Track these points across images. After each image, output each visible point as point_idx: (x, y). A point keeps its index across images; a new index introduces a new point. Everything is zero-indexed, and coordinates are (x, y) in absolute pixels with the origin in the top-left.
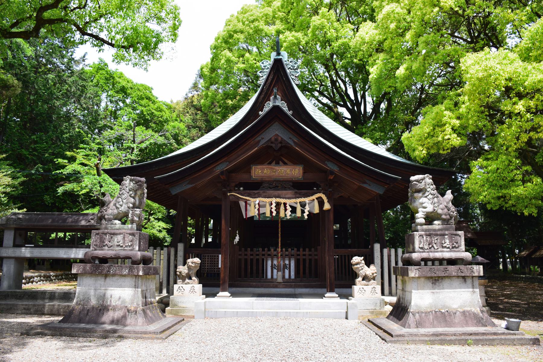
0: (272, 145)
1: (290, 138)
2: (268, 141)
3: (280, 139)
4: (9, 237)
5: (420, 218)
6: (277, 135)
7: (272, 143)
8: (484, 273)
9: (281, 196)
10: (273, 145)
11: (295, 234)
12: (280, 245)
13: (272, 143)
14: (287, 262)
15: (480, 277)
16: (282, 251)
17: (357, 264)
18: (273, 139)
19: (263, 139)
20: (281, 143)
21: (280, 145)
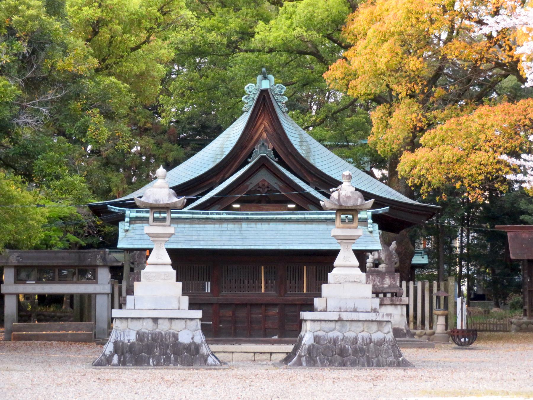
0: (259, 189)
1: (276, 183)
2: (256, 186)
3: (266, 184)
4: (8, 275)
6: (264, 180)
7: (259, 187)
8: (276, 335)
13: (259, 187)
15: (104, 355)
18: (261, 185)
19: (251, 184)
20: (268, 187)
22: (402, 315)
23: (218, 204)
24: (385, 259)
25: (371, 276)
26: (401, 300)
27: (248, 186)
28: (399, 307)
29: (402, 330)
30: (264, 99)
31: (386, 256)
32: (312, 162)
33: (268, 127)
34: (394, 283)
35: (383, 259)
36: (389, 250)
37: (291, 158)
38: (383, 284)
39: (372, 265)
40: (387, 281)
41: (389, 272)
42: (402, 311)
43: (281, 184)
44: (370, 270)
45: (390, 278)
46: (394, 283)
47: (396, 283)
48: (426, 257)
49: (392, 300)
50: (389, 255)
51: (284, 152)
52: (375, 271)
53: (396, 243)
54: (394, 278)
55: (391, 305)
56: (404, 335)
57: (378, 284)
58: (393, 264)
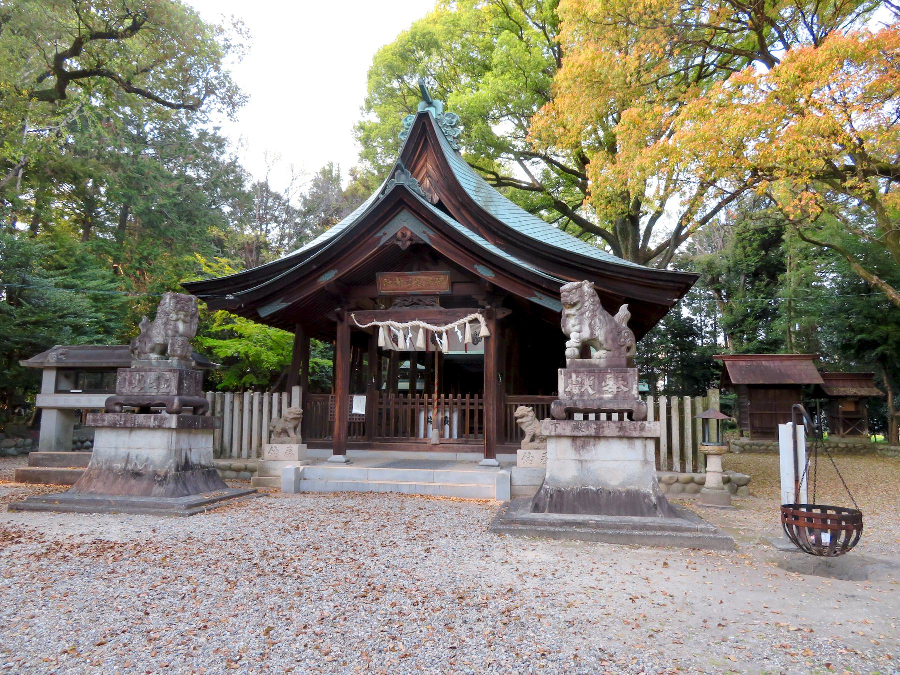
1: (424, 232)
3: (409, 234)
5: (572, 348)
6: (406, 228)
7: (399, 240)
9: (414, 322)
10: (400, 244)
11: (456, 377)
12: (436, 389)
13: (399, 240)
14: (448, 415)
16: (439, 397)
17: (523, 417)
19: (385, 234)
20: (411, 240)
21: (409, 243)
22: (646, 462)
23: (332, 269)
24: (606, 340)
25: (574, 376)
26: (642, 429)
27: (380, 238)
28: (639, 444)
29: (647, 496)
30: (424, 130)
31: (608, 333)
32: (493, 213)
33: (432, 171)
34: (626, 390)
35: (601, 339)
36: (612, 321)
37: (464, 212)
38: (600, 392)
39: (577, 352)
40: (611, 386)
41: (618, 368)
42: (645, 452)
43: (431, 234)
44: (572, 364)
45: (616, 378)
46: (626, 390)
47: (631, 390)
48: (647, 385)
49: (621, 429)
50: (615, 332)
51: (454, 205)
52: (583, 365)
53: (629, 309)
54: (624, 379)
55: (621, 438)
56: (652, 510)
57: (591, 392)
58: (624, 349)
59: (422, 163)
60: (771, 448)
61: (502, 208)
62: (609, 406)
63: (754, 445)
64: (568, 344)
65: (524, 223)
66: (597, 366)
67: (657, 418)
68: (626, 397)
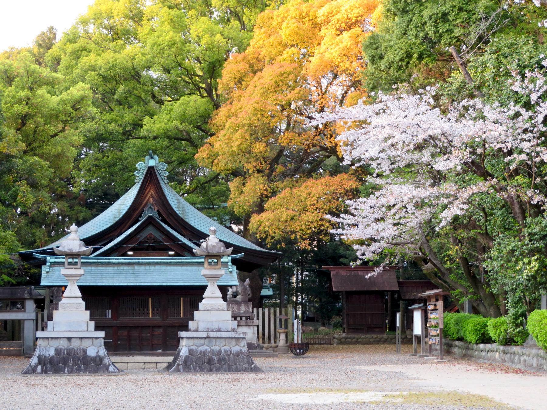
6: (151, 234)
20: (154, 239)
22: (254, 333)
26: (253, 322)
27: (139, 238)
28: (252, 327)
29: (254, 344)
32: (187, 220)
35: (240, 291)
36: (243, 285)
37: (171, 217)
38: (239, 310)
41: (244, 302)
49: (246, 322)
50: (245, 289)
52: (234, 301)
54: (247, 306)
55: (246, 325)
56: (256, 348)
59: (148, 190)
60: (360, 340)
61: (191, 216)
62: (242, 315)
63: (348, 338)
64: (228, 293)
65: (202, 225)
66: (238, 301)
67: (258, 318)
68: (248, 312)
